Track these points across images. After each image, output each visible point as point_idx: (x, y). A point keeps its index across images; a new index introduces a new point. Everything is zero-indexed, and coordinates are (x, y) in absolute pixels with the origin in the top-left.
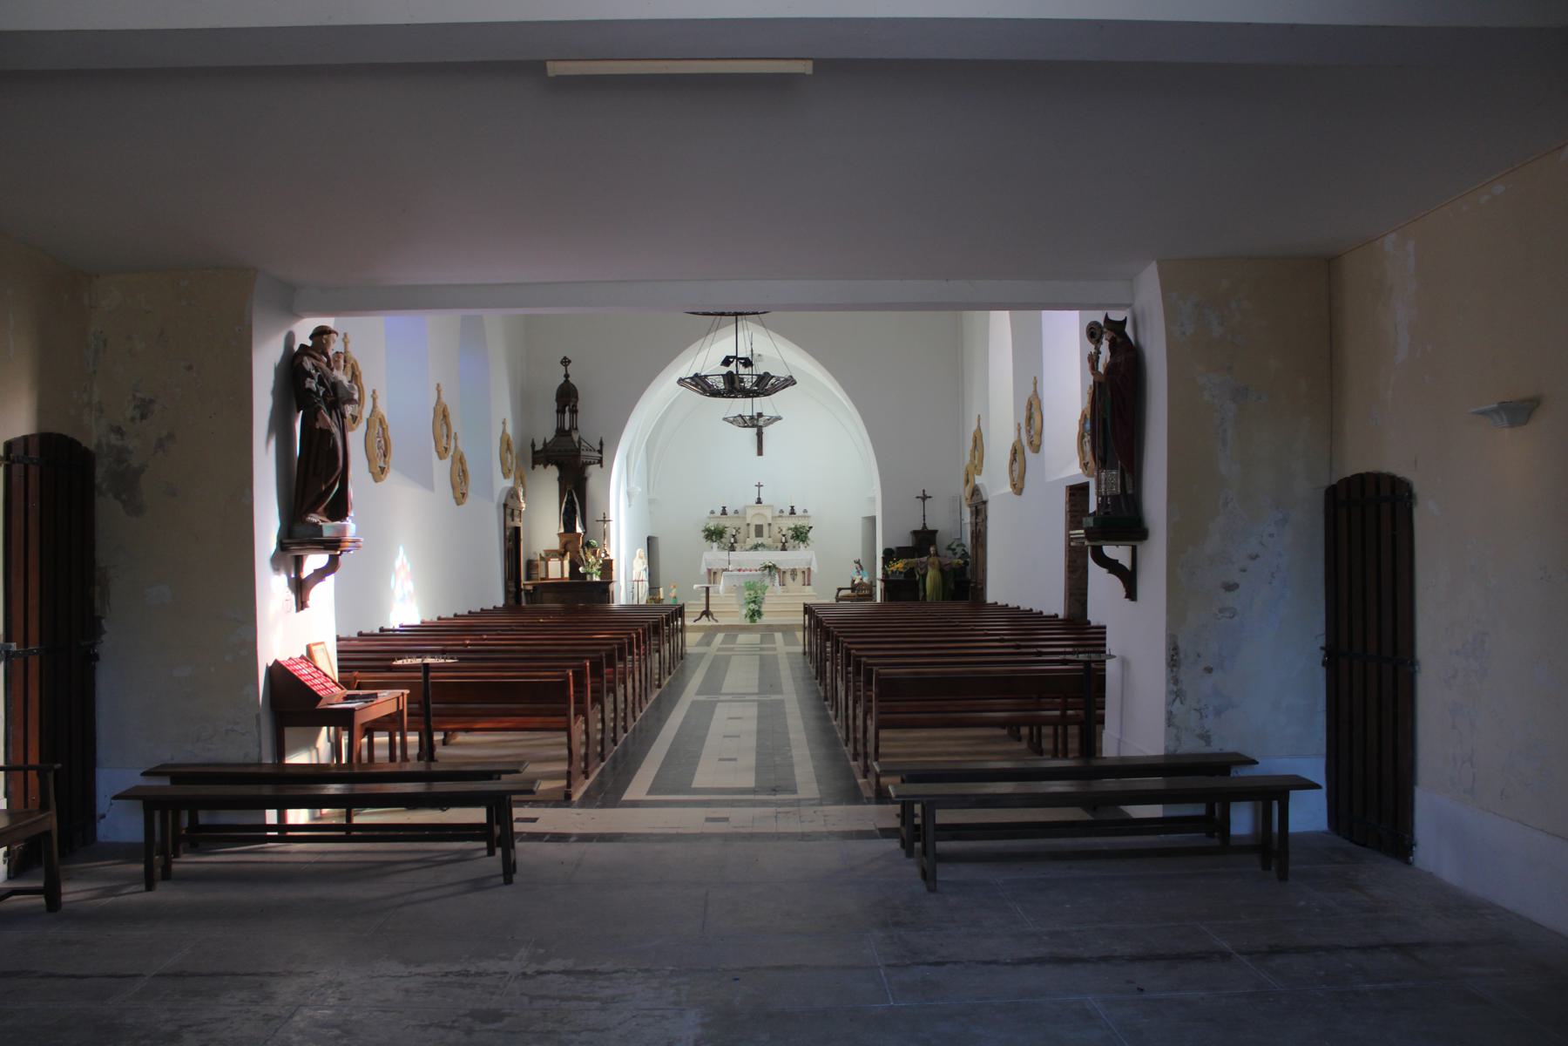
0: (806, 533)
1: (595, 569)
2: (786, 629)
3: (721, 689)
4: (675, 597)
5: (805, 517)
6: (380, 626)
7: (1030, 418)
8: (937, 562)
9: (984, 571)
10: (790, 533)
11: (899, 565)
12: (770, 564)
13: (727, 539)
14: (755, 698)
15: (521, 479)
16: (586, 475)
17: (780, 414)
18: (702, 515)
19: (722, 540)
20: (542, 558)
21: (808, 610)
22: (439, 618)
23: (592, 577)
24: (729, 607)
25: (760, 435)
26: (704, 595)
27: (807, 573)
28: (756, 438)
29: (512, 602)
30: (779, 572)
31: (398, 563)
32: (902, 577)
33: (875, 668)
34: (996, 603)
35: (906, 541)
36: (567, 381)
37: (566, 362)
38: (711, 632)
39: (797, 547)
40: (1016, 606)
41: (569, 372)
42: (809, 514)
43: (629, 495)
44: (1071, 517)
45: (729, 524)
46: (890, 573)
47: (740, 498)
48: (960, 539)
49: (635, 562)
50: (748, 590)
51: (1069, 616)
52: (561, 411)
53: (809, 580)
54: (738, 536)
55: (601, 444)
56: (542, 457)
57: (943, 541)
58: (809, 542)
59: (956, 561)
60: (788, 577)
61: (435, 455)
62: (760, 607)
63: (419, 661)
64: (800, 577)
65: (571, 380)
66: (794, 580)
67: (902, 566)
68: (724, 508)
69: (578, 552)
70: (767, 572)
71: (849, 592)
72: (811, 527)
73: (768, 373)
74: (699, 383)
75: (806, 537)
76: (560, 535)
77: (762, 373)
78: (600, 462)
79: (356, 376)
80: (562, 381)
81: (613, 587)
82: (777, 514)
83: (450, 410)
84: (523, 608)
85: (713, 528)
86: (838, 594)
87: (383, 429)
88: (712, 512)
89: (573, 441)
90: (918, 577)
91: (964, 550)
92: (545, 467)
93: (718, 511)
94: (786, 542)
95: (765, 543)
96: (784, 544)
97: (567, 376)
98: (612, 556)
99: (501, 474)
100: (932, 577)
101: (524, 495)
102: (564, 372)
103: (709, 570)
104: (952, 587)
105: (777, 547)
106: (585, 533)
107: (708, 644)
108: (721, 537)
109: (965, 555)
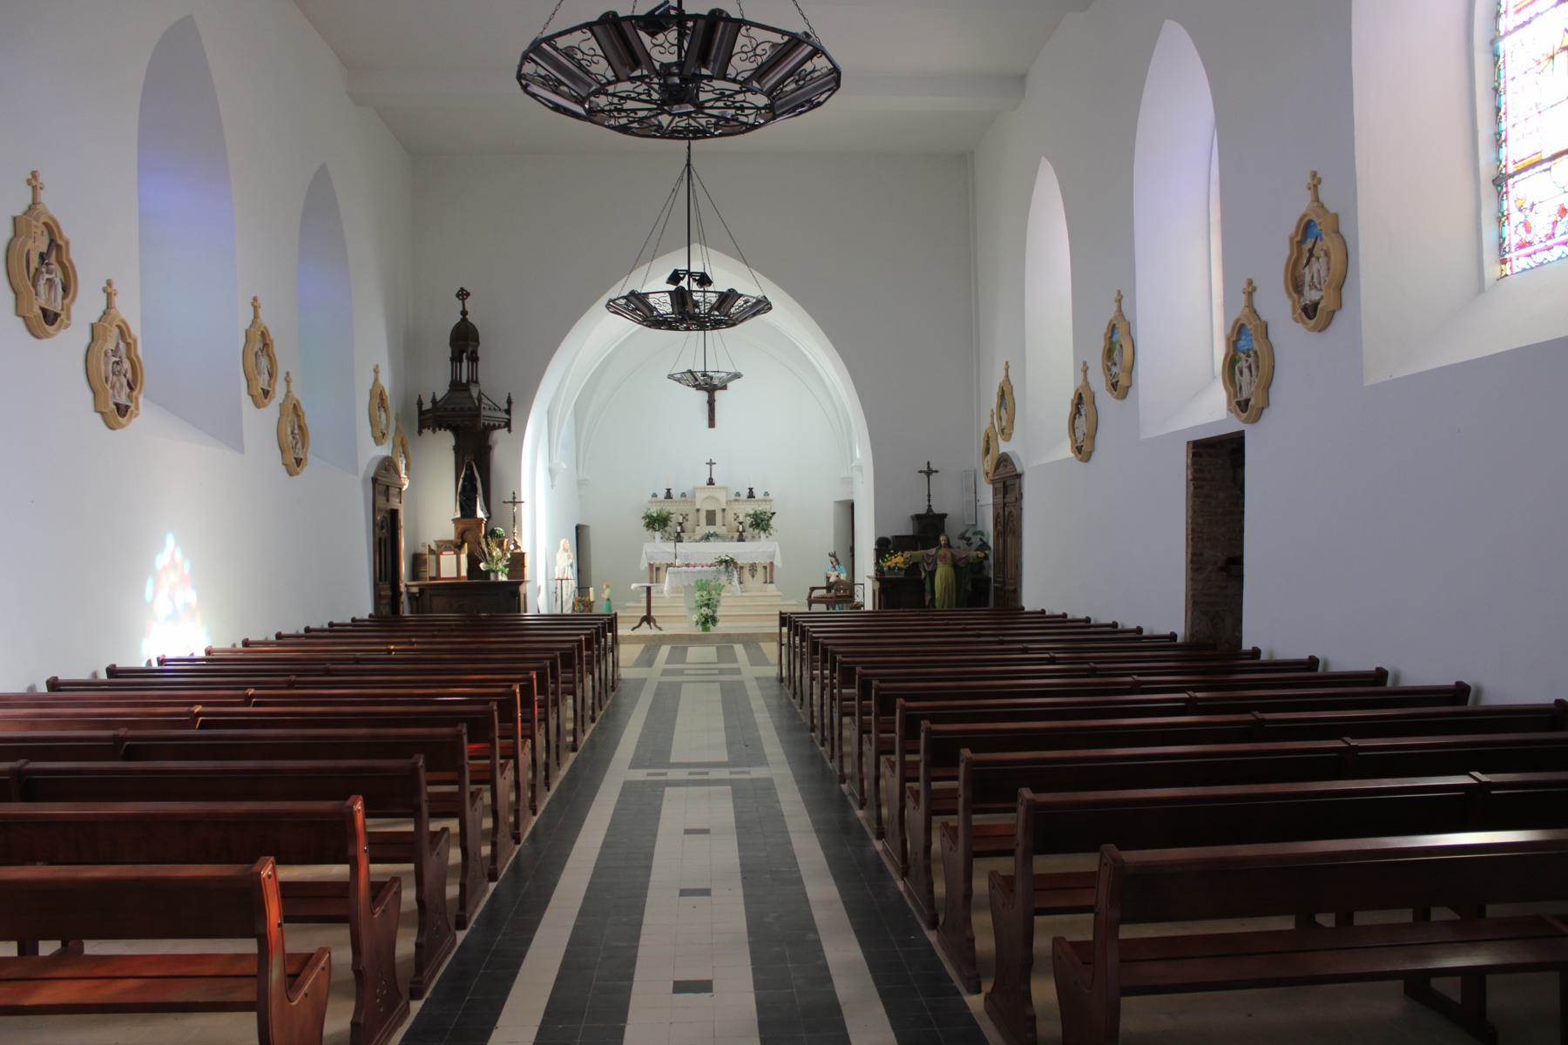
0: (768, 521)
1: (500, 566)
2: (750, 641)
3: (668, 753)
4: (608, 599)
5: (766, 501)
6: (351, 617)
7: (1109, 353)
8: (949, 556)
9: (1018, 567)
10: (749, 520)
11: (898, 560)
12: (727, 558)
13: (673, 527)
14: (724, 774)
15: (403, 447)
16: (490, 443)
17: (739, 370)
18: (645, 501)
19: (666, 528)
20: (431, 551)
21: (785, 619)
22: (246, 643)
23: (497, 577)
24: (676, 614)
25: (711, 403)
26: (645, 595)
27: (769, 568)
29: (386, 611)
30: (736, 568)
31: (162, 560)
32: (902, 575)
34: (1043, 612)
35: (905, 528)
36: (464, 320)
37: (463, 295)
38: (653, 644)
39: (757, 537)
40: (1039, 609)
41: (467, 308)
42: (771, 497)
44: (1195, 488)
45: (675, 509)
46: (885, 569)
47: (688, 478)
48: (975, 525)
50: (699, 590)
51: (1192, 635)
52: (456, 359)
53: (771, 577)
54: (687, 525)
55: (509, 402)
56: (432, 417)
57: (953, 528)
58: (771, 531)
59: (975, 553)
60: (746, 573)
61: (247, 400)
62: (714, 612)
64: (760, 573)
65: (470, 318)
66: (753, 576)
67: (902, 560)
68: (669, 490)
69: (479, 543)
70: (723, 567)
71: (824, 592)
72: (773, 514)
73: (734, 290)
74: (637, 306)
75: (768, 525)
76: (455, 521)
77: (725, 290)
78: (508, 425)
79: (59, 247)
80: (459, 320)
81: (527, 589)
82: (733, 497)
83: (273, 335)
84: (404, 619)
85: (655, 515)
86: (811, 594)
87: (128, 345)
88: (655, 495)
89: (472, 397)
90: (923, 574)
91: (981, 540)
92: (434, 431)
93: (662, 494)
94: (744, 531)
95: (718, 532)
96: (741, 533)
97: (464, 313)
98: (525, 547)
99: (372, 439)
100: (942, 574)
101: (407, 468)
102: (461, 309)
103: (651, 566)
104: (969, 587)
105: (733, 537)
106: (488, 518)
107: (650, 663)
108: (666, 525)
109: (984, 546)
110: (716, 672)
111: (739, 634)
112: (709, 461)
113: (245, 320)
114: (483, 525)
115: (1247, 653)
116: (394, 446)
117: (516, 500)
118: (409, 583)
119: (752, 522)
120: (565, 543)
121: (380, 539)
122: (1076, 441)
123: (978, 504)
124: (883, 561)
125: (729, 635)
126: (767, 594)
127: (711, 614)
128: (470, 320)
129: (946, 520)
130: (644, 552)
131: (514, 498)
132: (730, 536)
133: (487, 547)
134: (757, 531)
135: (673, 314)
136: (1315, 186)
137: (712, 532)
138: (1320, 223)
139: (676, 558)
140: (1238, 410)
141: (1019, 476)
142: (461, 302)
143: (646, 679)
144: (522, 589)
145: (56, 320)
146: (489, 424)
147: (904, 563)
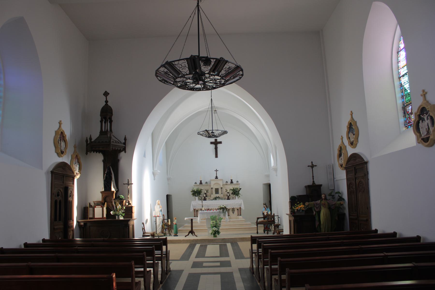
0: (238, 192)
2: (234, 242)
4: (176, 224)
5: (237, 184)
10: (231, 192)
11: (301, 206)
12: (223, 207)
13: (203, 195)
15: (76, 158)
18: (191, 185)
19: (200, 195)
23: (119, 217)
25: (216, 149)
27: (239, 210)
28: (214, 150)
30: (227, 211)
32: (303, 214)
33: (257, 239)
35: (301, 191)
37: (106, 94)
39: (234, 198)
41: (108, 100)
42: (239, 183)
43: (154, 174)
46: (296, 211)
49: (156, 207)
53: (240, 213)
54: (208, 194)
55: (125, 139)
57: (325, 191)
58: (240, 195)
60: (231, 212)
62: (218, 229)
63: (25, 264)
64: (236, 212)
65: (109, 104)
66: (233, 213)
68: (201, 181)
70: (221, 210)
72: (240, 189)
73: (223, 58)
75: (239, 193)
76: (102, 192)
80: (104, 105)
82: (225, 183)
88: (196, 183)
90: (314, 213)
91: (339, 196)
93: (198, 183)
94: (229, 196)
96: (228, 197)
97: (107, 102)
99: (56, 154)
100: (323, 212)
102: (105, 100)
104: (337, 218)
105: (225, 198)
106: (117, 192)
108: (200, 194)
110: (218, 264)
111: (229, 239)
112: (216, 170)
113: (56, 127)
114: (114, 194)
115: (373, 231)
116: (72, 158)
117: (129, 183)
118: (79, 221)
119: (232, 192)
120: (158, 201)
121: (56, 201)
122: (421, 135)
123: (335, 180)
124: (294, 207)
125: (225, 239)
126: (238, 220)
127: (217, 230)
128: (109, 105)
129: (321, 187)
130: (192, 205)
131: (128, 182)
132: (224, 198)
133: (115, 204)
134: (234, 196)
135: (190, 74)
136: (424, 95)
137: (217, 196)
138: (428, 108)
139: (202, 207)
140: (423, 142)
141: (366, 163)
142: (105, 97)
143: (183, 271)
144: (131, 223)
145: (63, 153)
146: (118, 149)
147: (304, 208)
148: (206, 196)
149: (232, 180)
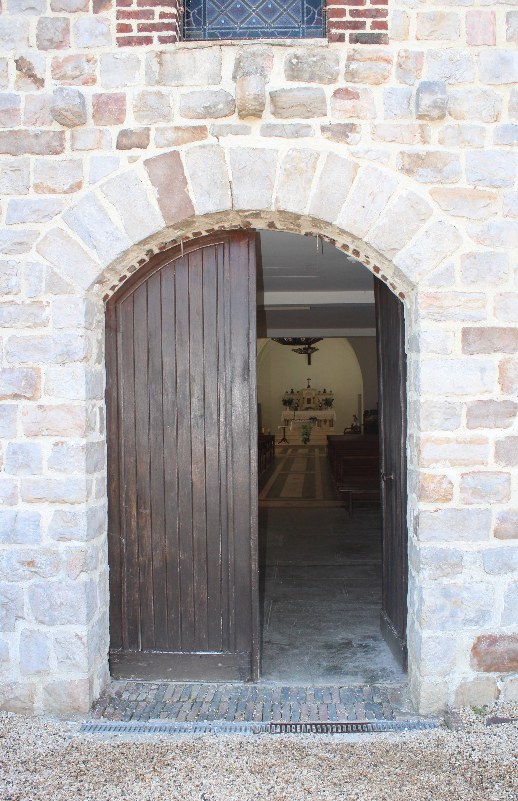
5: (330, 394)
10: (324, 402)
13: (294, 405)
54: (299, 404)
60: (323, 423)
64: (328, 423)
70: (312, 421)
72: (333, 400)
82: (317, 393)
88: (287, 392)
93: (289, 392)
148: (298, 406)
149: (325, 390)
